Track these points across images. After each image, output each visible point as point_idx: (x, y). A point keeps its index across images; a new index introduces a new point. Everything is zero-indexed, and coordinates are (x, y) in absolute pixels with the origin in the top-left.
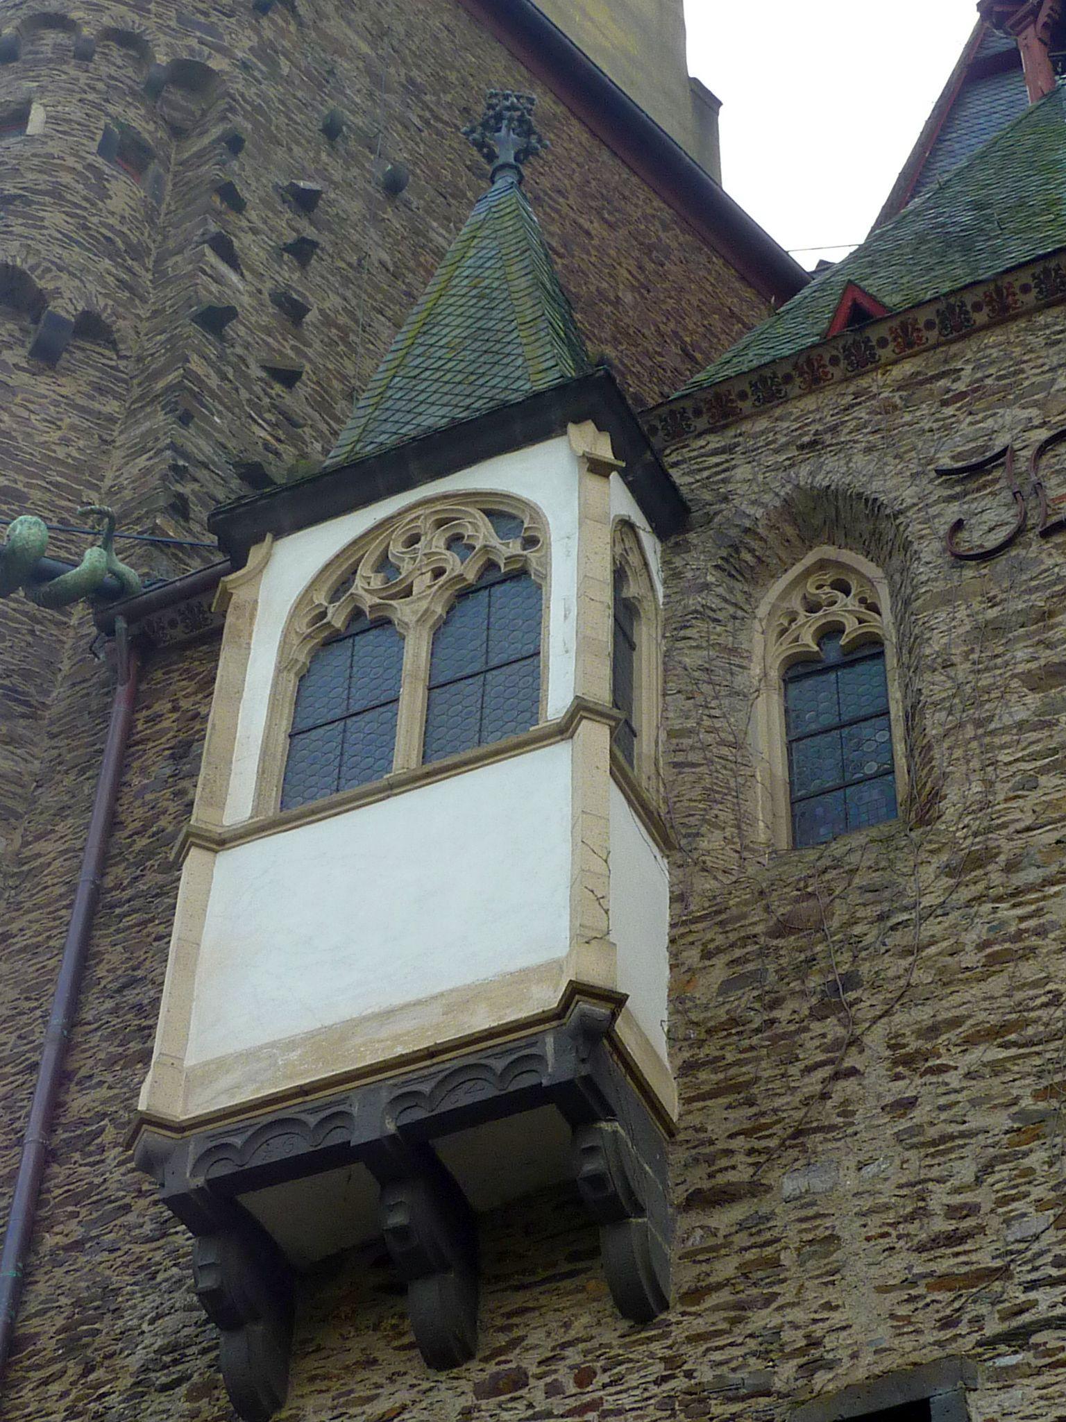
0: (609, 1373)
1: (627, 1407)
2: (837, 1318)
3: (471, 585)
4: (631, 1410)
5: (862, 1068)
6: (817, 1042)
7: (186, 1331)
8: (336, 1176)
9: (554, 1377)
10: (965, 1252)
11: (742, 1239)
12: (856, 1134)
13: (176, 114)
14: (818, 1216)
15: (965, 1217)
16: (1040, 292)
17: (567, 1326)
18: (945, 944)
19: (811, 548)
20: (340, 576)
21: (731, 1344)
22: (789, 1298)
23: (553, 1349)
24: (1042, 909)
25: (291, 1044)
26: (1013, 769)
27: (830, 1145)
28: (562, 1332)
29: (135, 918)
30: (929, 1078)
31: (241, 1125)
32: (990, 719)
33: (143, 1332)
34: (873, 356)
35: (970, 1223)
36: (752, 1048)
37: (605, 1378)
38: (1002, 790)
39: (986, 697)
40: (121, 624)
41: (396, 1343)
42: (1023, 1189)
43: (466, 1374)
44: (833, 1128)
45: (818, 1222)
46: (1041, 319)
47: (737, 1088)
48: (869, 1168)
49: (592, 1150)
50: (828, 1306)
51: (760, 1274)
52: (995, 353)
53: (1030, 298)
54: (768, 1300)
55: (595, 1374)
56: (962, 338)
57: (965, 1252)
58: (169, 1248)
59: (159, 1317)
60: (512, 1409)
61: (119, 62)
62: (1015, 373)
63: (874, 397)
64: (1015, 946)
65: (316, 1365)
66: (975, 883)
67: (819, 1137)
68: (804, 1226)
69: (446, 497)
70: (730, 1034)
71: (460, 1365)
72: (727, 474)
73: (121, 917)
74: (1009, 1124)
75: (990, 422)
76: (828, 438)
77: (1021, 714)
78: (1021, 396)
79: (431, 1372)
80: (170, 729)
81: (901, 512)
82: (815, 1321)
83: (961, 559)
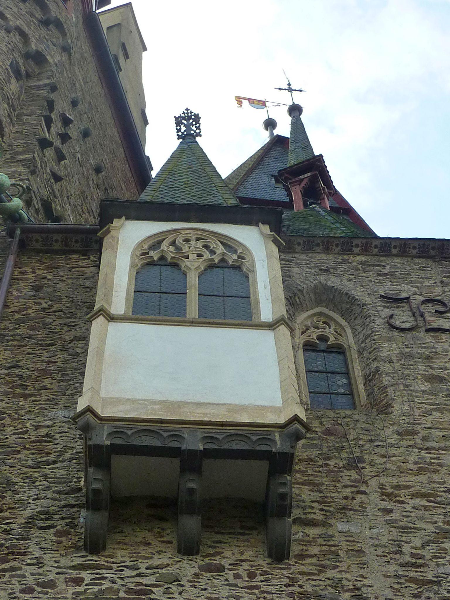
0: (263, 577)
1: (273, 592)
2: (366, 582)
3: (215, 264)
4: (275, 593)
5: (368, 493)
6: (348, 478)
7: (53, 508)
8: (165, 461)
9: (237, 571)
10: (420, 572)
11: (321, 541)
12: (368, 515)
13: (29, 69)
14: (354, 541)
15: (419, 559)
16: (419, 251)
17: (242, 553)
18: (400, 458)
19: (317, 307)
20: (156, 242)
21: (320, 580)
22: (343, 569)
23: (236, 560)
24: (440, 457)
25: (154, 402)
26: (422, 405)
27: (357, 517)
28: (241, 555)
29: (16, 343)
30: (396, 504)
31: (130, 426)
32: (410, 386)
33: (29, 503)
34: (351, 249)
35: (419, 561)
36: (320, 472)
37: (262, 578)
38: (417, 412)
39: (408, 378)
40: (18, 232)
41: (159, 539)
42: (443, 555)
43: (195, 560)
44: (358, 511)
45: (355, 544)
46: (417, 260)
47: (315, 485)
48: (375, 530)
49: (284, 484)
50: (362, 576)
51: (331, 557)
52: (399, 265)
53: (414, 252)
54: (335, 567)
55: (256, 575)
56: (385, 256)
57: (420, 572)
58: (41, 473)
59: (38, 499)
60: (218, 579)
61: (18, 40)
62: (408, 274)
63: (350, 263)
64: (431, 467)
65: (120, 538)
66: (410, 440)
67: (352, 512)
68: (348, 543)
69: (203, 230)
70: (309, 464)
71: (194, 556)
72: (289, 269)
73: (9, 341)
74: (434, 530)
75: (398, 287)
76: (332, 270)
77: (423, 388)
78: (411, 283)
79: (179, 555)
80: (30, 279)
81: (365, 305)
82: (357, 580)
83: (393, 327)
